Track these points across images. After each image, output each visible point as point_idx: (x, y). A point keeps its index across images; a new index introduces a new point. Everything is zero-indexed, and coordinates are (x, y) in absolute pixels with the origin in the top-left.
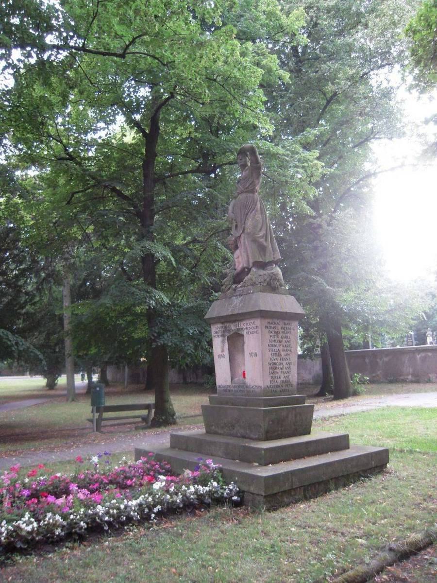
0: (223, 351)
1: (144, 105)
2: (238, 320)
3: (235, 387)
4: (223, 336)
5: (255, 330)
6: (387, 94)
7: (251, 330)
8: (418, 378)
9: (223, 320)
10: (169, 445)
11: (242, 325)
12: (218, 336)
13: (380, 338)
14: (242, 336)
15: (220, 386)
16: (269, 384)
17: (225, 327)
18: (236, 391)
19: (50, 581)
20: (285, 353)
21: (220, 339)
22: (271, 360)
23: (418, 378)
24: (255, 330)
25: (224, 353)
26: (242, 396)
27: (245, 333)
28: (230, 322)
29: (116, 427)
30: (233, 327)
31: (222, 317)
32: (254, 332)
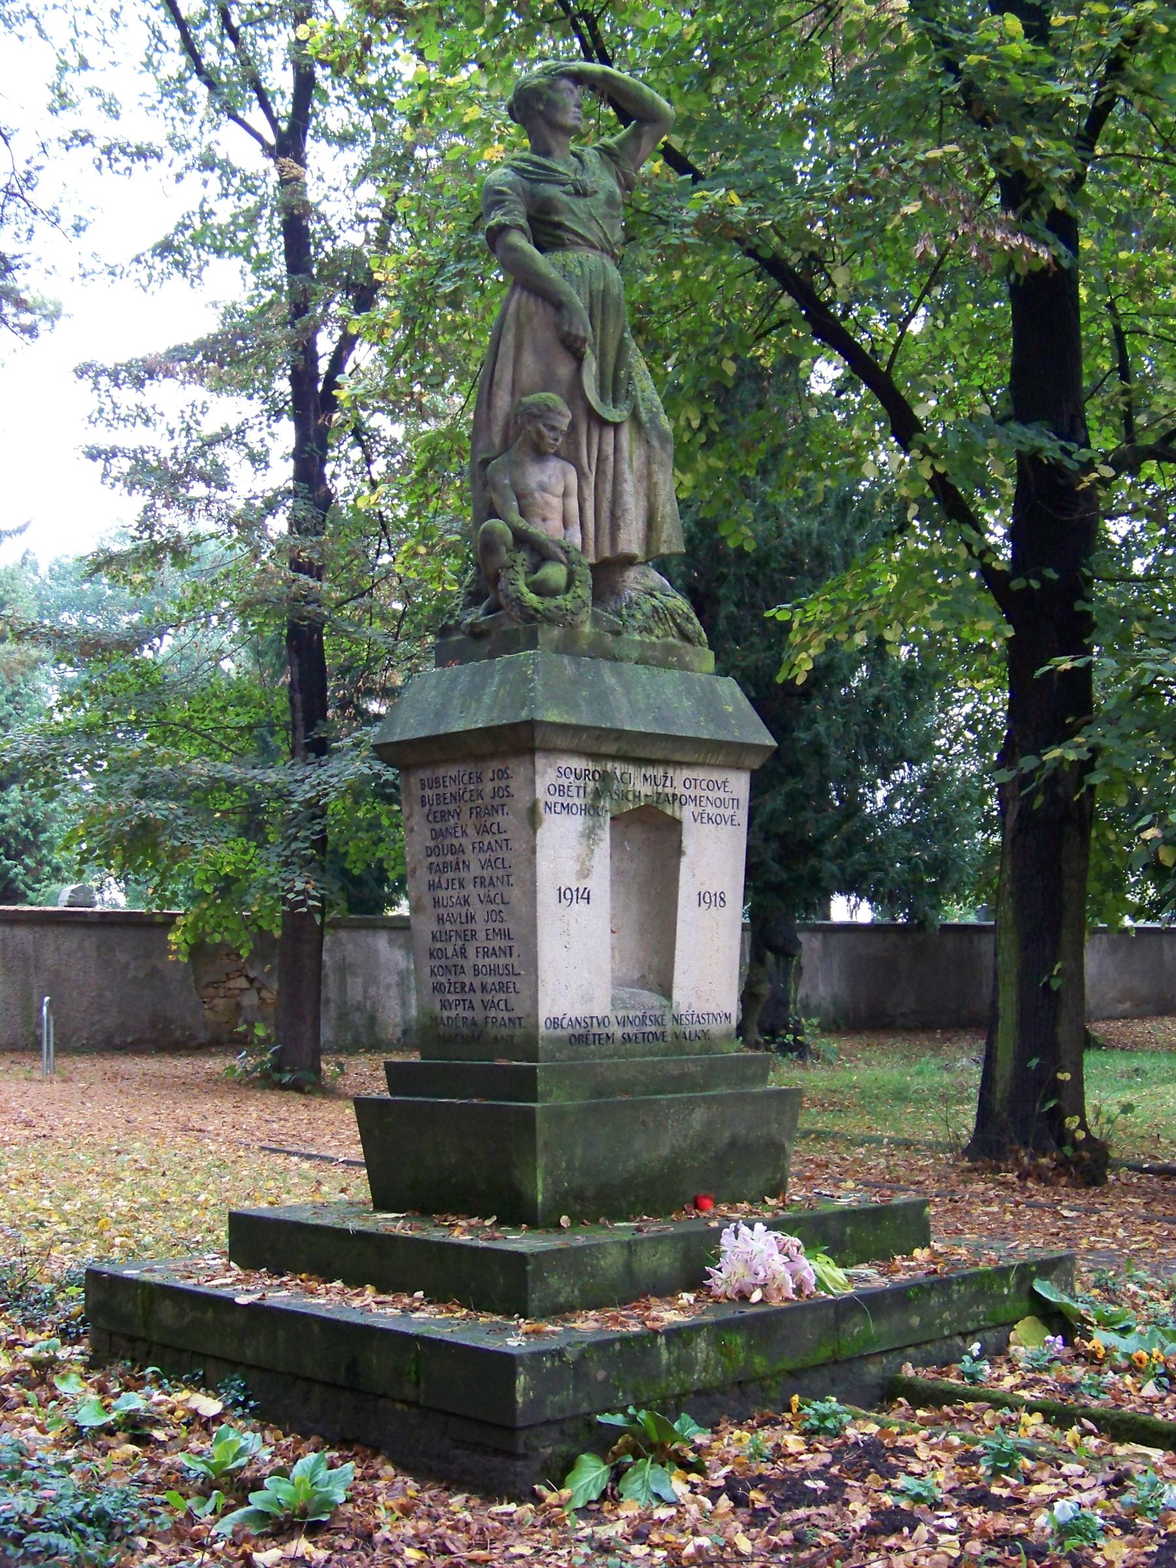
0: (584, 873)
2: (666, 763)
3: (622, 1022)
4: (592, 810)
5: (728, 813)
7: (711, 810)
8: (839, 563)
9: (612, 749)
11: (679, 780)
12: (567, 808)
13: (798, 131)
14: (676, 824)
15: (555, 1023)
18: (627, 1039)
20: (483, 857)
21: (576, 823)
23: (839, 563)
24: (728, 813)
25: (590, 883)
26: (652, 1054)
27: (686, 814)
28: (640, 762)
29: (295, 1159)
31: (620, 735)
32: (722, 817)
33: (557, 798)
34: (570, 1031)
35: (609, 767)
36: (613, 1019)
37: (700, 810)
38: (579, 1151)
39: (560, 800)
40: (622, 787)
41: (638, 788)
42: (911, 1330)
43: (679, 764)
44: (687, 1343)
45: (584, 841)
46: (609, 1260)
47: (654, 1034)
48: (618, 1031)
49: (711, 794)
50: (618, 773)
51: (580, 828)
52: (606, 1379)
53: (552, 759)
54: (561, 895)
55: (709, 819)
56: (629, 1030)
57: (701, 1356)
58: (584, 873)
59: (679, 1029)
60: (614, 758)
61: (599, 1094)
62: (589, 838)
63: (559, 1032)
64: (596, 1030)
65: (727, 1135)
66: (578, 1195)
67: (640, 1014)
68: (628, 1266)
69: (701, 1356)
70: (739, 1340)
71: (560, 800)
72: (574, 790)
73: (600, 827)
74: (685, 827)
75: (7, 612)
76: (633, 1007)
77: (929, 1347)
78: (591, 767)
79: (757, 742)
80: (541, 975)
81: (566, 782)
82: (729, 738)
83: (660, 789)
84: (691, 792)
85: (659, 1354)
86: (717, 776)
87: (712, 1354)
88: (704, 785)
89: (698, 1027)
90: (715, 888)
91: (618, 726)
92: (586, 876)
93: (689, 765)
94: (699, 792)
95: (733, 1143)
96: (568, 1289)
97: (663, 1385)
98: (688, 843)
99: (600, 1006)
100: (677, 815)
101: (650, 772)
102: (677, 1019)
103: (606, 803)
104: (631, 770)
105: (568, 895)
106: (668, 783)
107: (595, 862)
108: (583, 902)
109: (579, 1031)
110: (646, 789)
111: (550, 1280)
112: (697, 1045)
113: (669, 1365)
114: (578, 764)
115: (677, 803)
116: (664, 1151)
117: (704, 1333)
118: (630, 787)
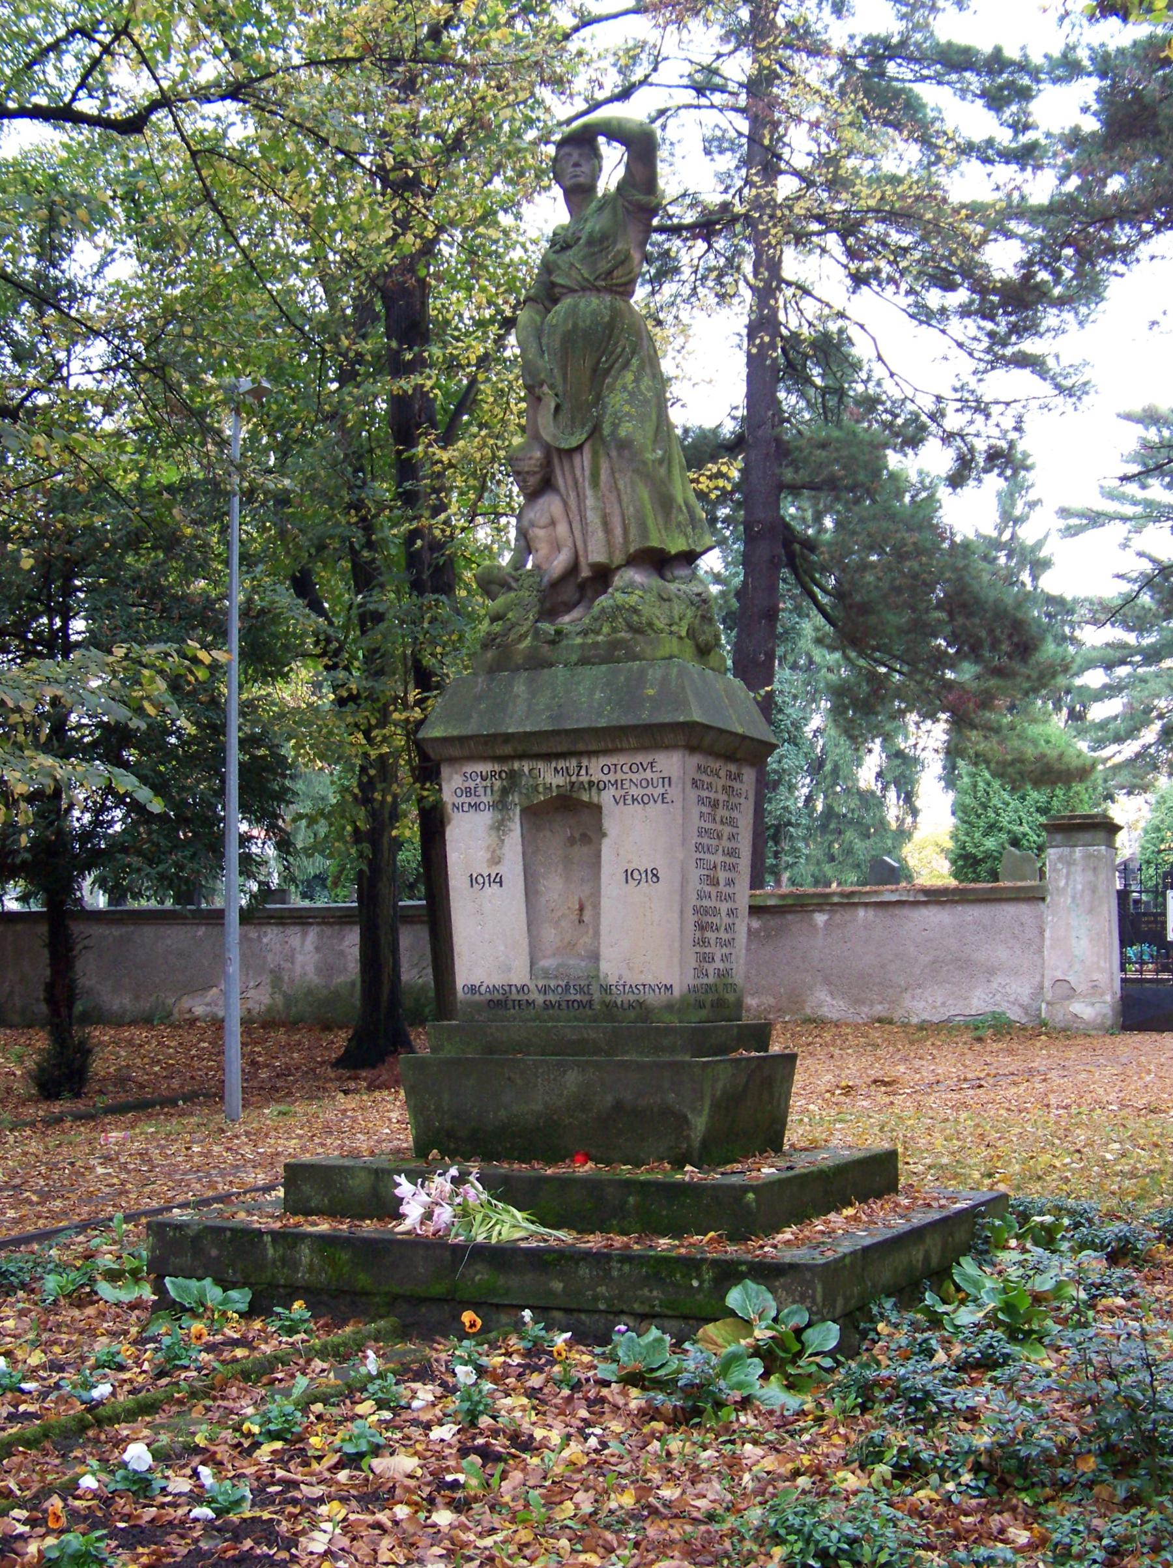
0: (496, 860)
1: (949, 645)
2: (580, 754)
3: (545, 990)
4: (501, 805)
6: (1147, 429)
7: (635, 791)
9: (508, 750)
10: (406, 1140)
11: (595, 768)
12: (476, 806)
14: (598, 808)
15: (473, 989)
16: (691, 981)
17: (513, 776)
18: (548, 1005)
19: (1169, 804)
21: (486, 818)
22: (700, 897)
25: (501, 869)
27: (606, 798)
28: (548, 757)
30: (550, 776)
31: (507, 738)
33: (464, 799)
34: (488, 997)
35: (516, 766)
36: (532, 987)
37: (623, 792)
38: (446, 1096)
39: (467, 800)
40: (531, 782)
41: (548, 780)
42: (551, 1293)
43: (596, 753)
44: (293, 1246)
45: (494, 833)
46: (357, 1181)
47: (580, 1003)
48: (540, 999)
49: (635, 777)
50: (526, 770)
51: (489, 822)
52: (218, 1257)
53: (457, 766)
54: (473, 880)
55: (634, 800)
56: (551, 997)
57: (305, 1261)
58: (496, 860)
59: (608, 998)
60: (521, 757)
61: (491, 1052)
62: (498, 829)
63: (477, 997)
64: (514, 996)
65: (609, 1099)
66: (450, 1134)
67: (563, 984)
68: (374, 1188)
69: (305, 1261)
70: (345, 1256)
71: (467, 800)
72: (481, 791)
73: (510, 819)
74: (605, 811)
75: (1167, 479)
76: (556, 977)
77: (583, 1316)
78: (497, 768)
79: (667, 720)
80: (457, 949)
81: (472, 784)
82: (634, 722)
83: (574, 778)
84: (612, 777)
85: (265, 1249)
86: (640, 758)
87: (316, 1261)
88: (626, 769)
89: (632, 998)
90: (645, 864)
91: (503, 730)
92: (498, 863)
93: (606, 752)
94: (620, 776)
95: (618, 1106)
96: (319, 1197)
97: (269, 1274)
98: (608, 824)
99: (519, 975)
100: (595, 800)
101: (561, 764)
102: (606, 989)
103: (514, 798)
104: (541, 765)
105: (480, 880)
106: (583, 772)
107: (506, 848)
108: (495, 887)
109: (497, 996)
110: (559, 780)
111: (304, 1188)
112: (632, 1014)
113: (274, 1262)
114: (485, 768)
115: (594, 790)
116: (538, 1107)
117: (308, 1241)
118: (540, 781)
